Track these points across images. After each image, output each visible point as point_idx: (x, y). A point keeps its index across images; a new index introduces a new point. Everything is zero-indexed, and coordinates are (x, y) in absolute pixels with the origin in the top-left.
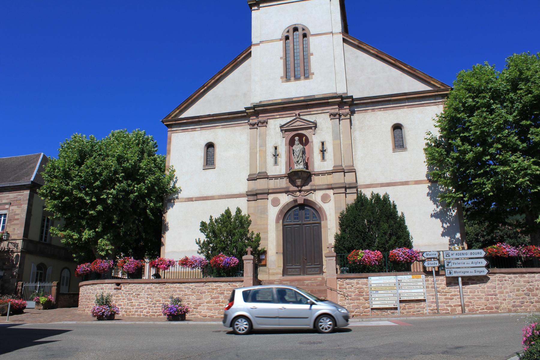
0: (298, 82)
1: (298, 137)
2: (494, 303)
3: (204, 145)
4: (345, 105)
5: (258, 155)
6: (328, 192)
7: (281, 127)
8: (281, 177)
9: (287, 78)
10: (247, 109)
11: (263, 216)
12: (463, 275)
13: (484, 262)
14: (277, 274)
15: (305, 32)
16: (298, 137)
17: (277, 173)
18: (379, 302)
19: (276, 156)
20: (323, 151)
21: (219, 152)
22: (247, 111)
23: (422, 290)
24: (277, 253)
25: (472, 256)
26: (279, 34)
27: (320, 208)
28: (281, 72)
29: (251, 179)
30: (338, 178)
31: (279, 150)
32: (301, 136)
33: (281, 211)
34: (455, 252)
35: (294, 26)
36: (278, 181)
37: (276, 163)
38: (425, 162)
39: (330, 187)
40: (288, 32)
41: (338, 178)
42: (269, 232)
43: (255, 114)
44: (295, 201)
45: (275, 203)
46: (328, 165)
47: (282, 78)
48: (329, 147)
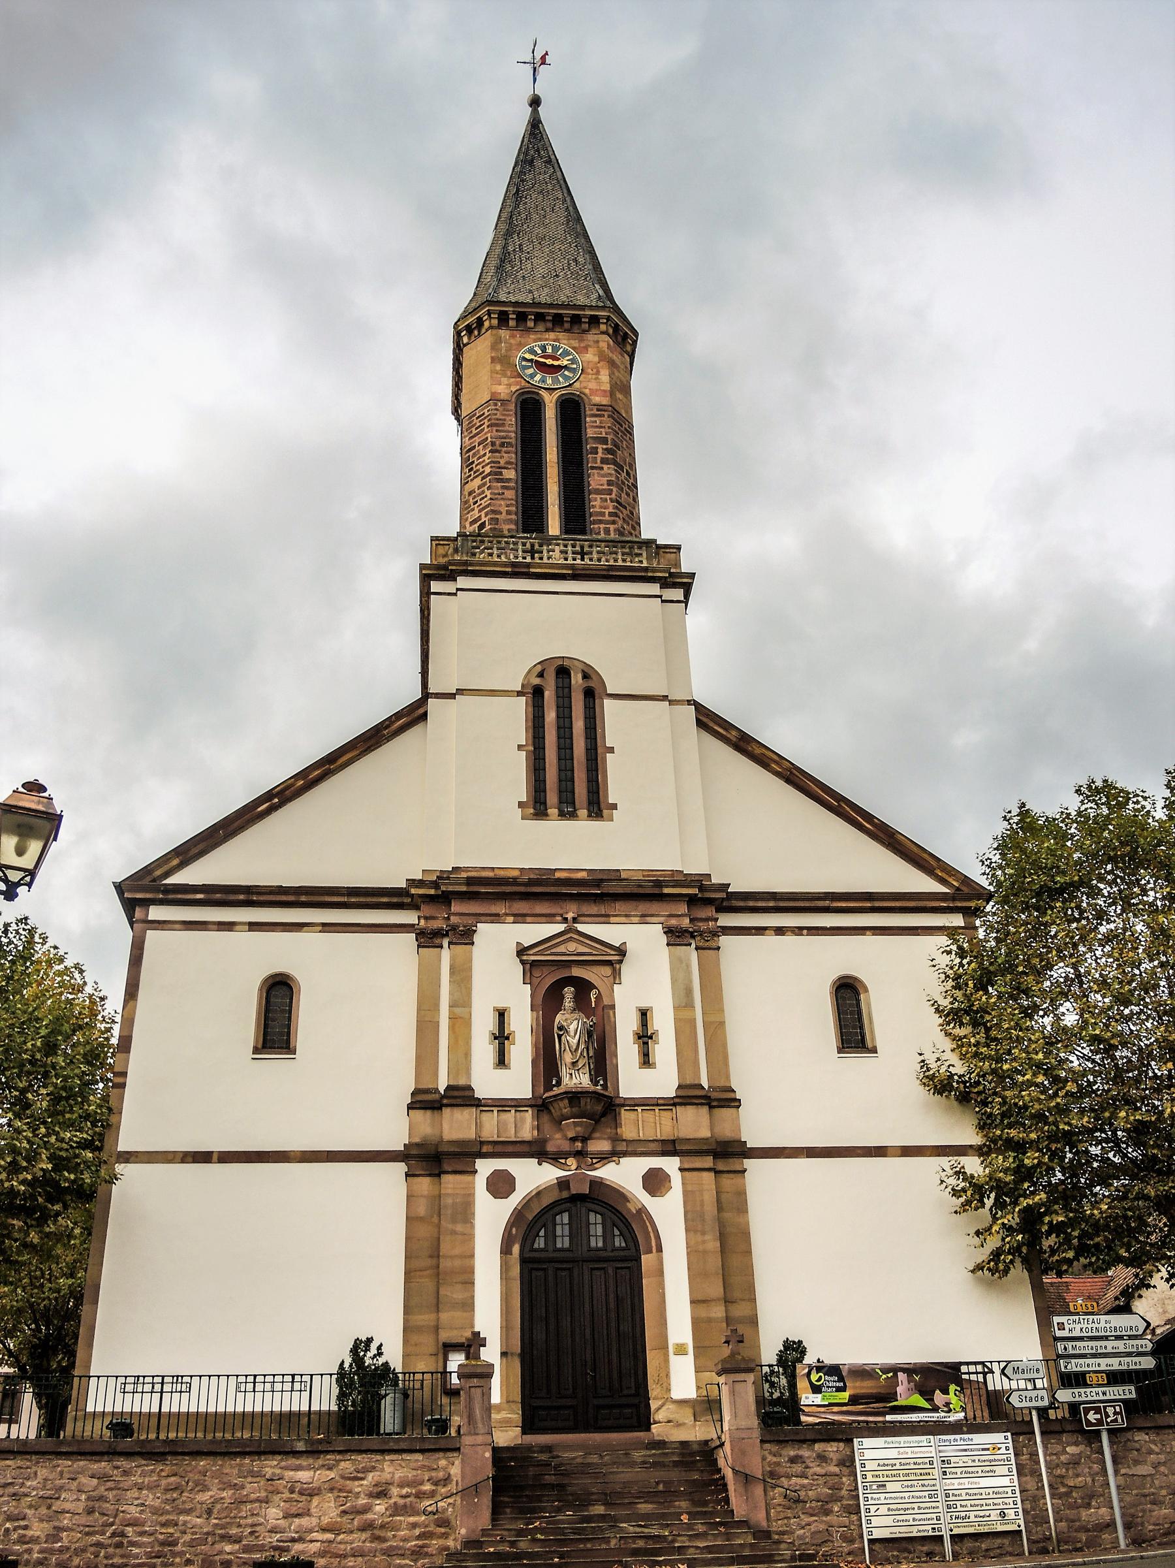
1: (566, 985)
4: (700, 909)
8: (517, 1105)
9: (537, 806)
10: (412, 882)
11: (459, 1228)
16: (566, 985)
18: (889, 1521)
19: (502, 1037)
22: (413, 891)
23: (1005, 1481)
27: (642, 1211)
30: (694, 1123)
33: (518, 1216)
36: (510, 1117)
39: (669, 1148)
40: (541, 675)
41: (694, 1123)
43: (444, 907)
45: (501, 1185)
46: (662, 1080)
48: (664, 1024)
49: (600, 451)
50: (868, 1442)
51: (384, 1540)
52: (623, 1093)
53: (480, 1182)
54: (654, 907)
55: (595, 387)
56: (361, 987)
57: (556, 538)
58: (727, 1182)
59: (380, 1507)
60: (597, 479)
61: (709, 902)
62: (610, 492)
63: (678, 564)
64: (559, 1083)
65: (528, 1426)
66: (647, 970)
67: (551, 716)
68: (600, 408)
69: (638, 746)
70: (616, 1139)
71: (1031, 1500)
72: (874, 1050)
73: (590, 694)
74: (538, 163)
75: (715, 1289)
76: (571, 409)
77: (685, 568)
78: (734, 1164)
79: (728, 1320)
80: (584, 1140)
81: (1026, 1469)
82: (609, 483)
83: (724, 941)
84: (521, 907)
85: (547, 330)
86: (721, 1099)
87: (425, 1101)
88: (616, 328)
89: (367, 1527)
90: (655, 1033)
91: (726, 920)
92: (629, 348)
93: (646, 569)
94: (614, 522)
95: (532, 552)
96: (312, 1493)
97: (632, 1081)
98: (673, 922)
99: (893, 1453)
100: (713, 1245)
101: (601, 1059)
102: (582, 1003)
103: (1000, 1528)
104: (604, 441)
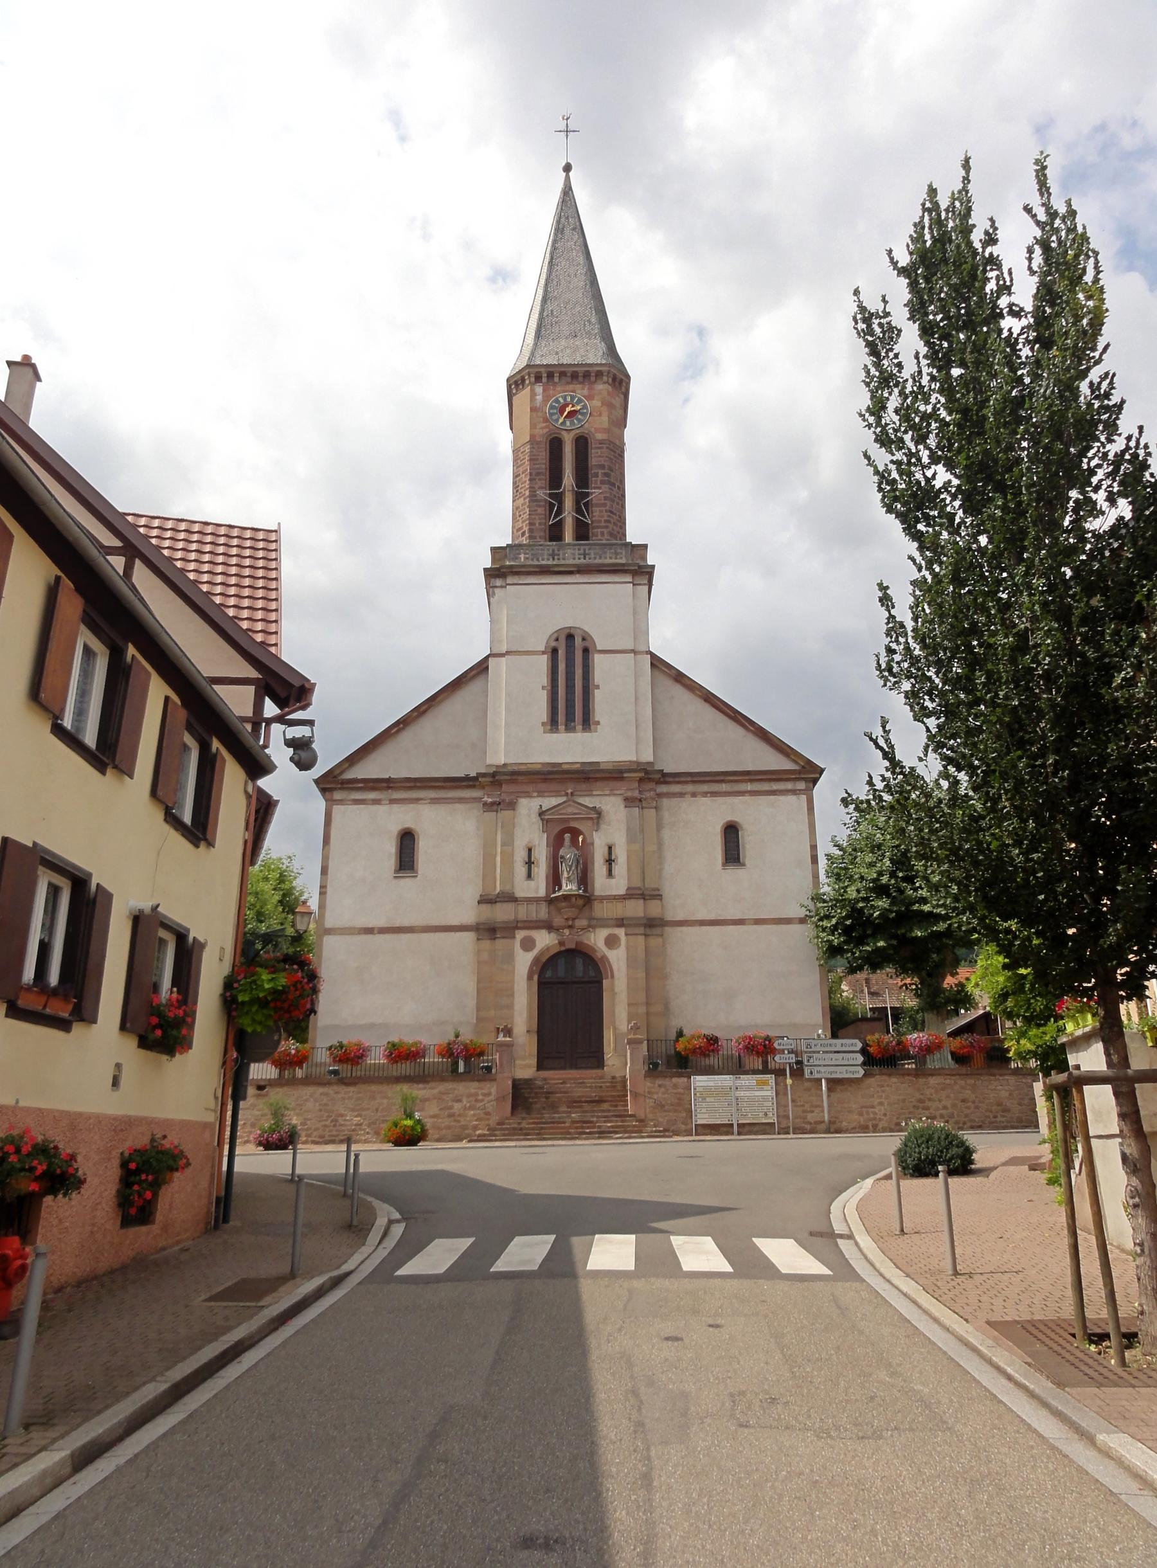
1: (564, 833)
2: (871, 1120)
3: (396, 833)
4: (647, 783)
5: (498, 859)
8: (537, 900)
9: (553, 723)
12: (829, 1076)
13: (860, 1059)
14: (529, 1066)
15: (587, 644)
18: (706, 1116)
19: (530, 863)
20: (610, 861)
21: (424, 849)
24: (528, 1031)
25: (844, 1049)
27: (604, 957)
28: (544, 716)
29: (485, 900)
30: (635, 909)
31: (535, 854)
32: (575, 833)
33: (536, 960)
34: (819, 1042)
36: (533, 907)
37: (529, 876)
39: (620, 923)
40: (557, 640)
41: (635, 909)
42: (516, 995)
43: (498, 786)
45: (528, 944)
46: (619, 885)
47: (543, 724)
48: (621, 855)
50: (698, 1078)
51: (459, 1121)
52: (597, 893)
54: (618, 784)
55: (597, 425)
56: (453, 836)
57: (569, 544)
58: (654, 942)
59: (457, 1106)
60: (596, 493)
61: (650, 780)
62: (605, 505)
63: (644, 558)
64: (560, 888)
65: (540, 1066)
66: (614, 825)
67: (562, 667)
68: (601, 442)
69: (614, 682)
70: (591, 919)
71: (781, 1106)
72: (744, 865)
73: (586, 651)
74: (567, 231)
75: (642, 998)
76: (582, 444)
77: (650, 563)
78: (658, 931)
79: (648, 1014)
80: (574, 919)
81: (780, 1092)
82: (606, 498)
83: (665, 802)
84: (543, 786)
85: (568, 383)
86: (655, 895)
88: (614, 379)
89: (451, 1115)
91: (663, 789)
92: (623, 389)
93: (623, 565)
94: (607, 527)
95: (553, 555)
96: (427, 1100)
97: (601, 884)
98: (629, 794)
99: (712, 1084)
100: (641, 975)
101: (584, 879)
103: (764, 1121)
104: (602, 467)
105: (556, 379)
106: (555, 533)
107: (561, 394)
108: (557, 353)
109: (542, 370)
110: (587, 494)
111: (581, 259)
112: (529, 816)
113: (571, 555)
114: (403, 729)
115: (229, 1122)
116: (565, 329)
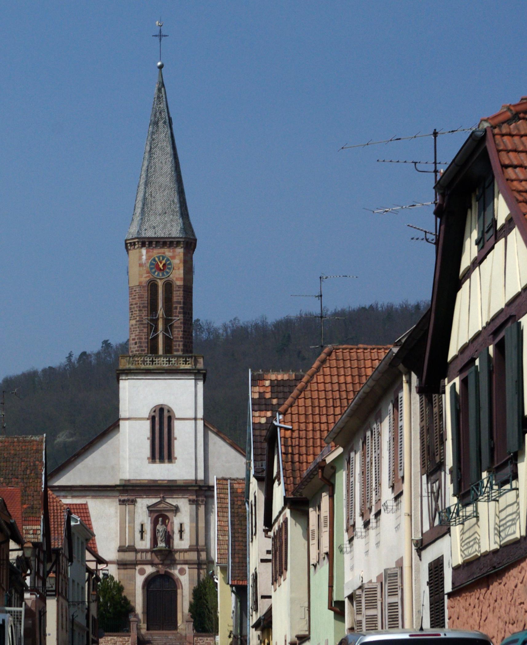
0: (162, 465)
1: (160, 516)
6: (184, 566)
7: (148, 507)
8: (146, 551)
9: (153, 458)
15: (170, 414)
17: (143, 547)
19: (142, 532)
20: (181, 531)
26: (146, 412)
27: (178, 579)
35: (161, 406)
37: (142, 538)
38: (49, 635)
39: (186, 563)
40: (155, 411)
41: (193, 556)
44: (158, 572)
45: (142, 572)
48: (187, 529)
49: (178, 308)
53: (137, 571)
66: (184, 513)
73: (170, 419)
87: (122, 549)
90: (184, 530)
97: (178, 544)
101: (168, 538)
102: (164, 523)
105: (154, 246)
106: (153, 349)
107: (156, 252)
108: (154, 228)
109: (146, 240)
110: (172, 320)
111: (169, 149)
112: (142, 508)
113: (162, 362)
114: (77, 458)
115: (284, 551)
116: (159, 208)
